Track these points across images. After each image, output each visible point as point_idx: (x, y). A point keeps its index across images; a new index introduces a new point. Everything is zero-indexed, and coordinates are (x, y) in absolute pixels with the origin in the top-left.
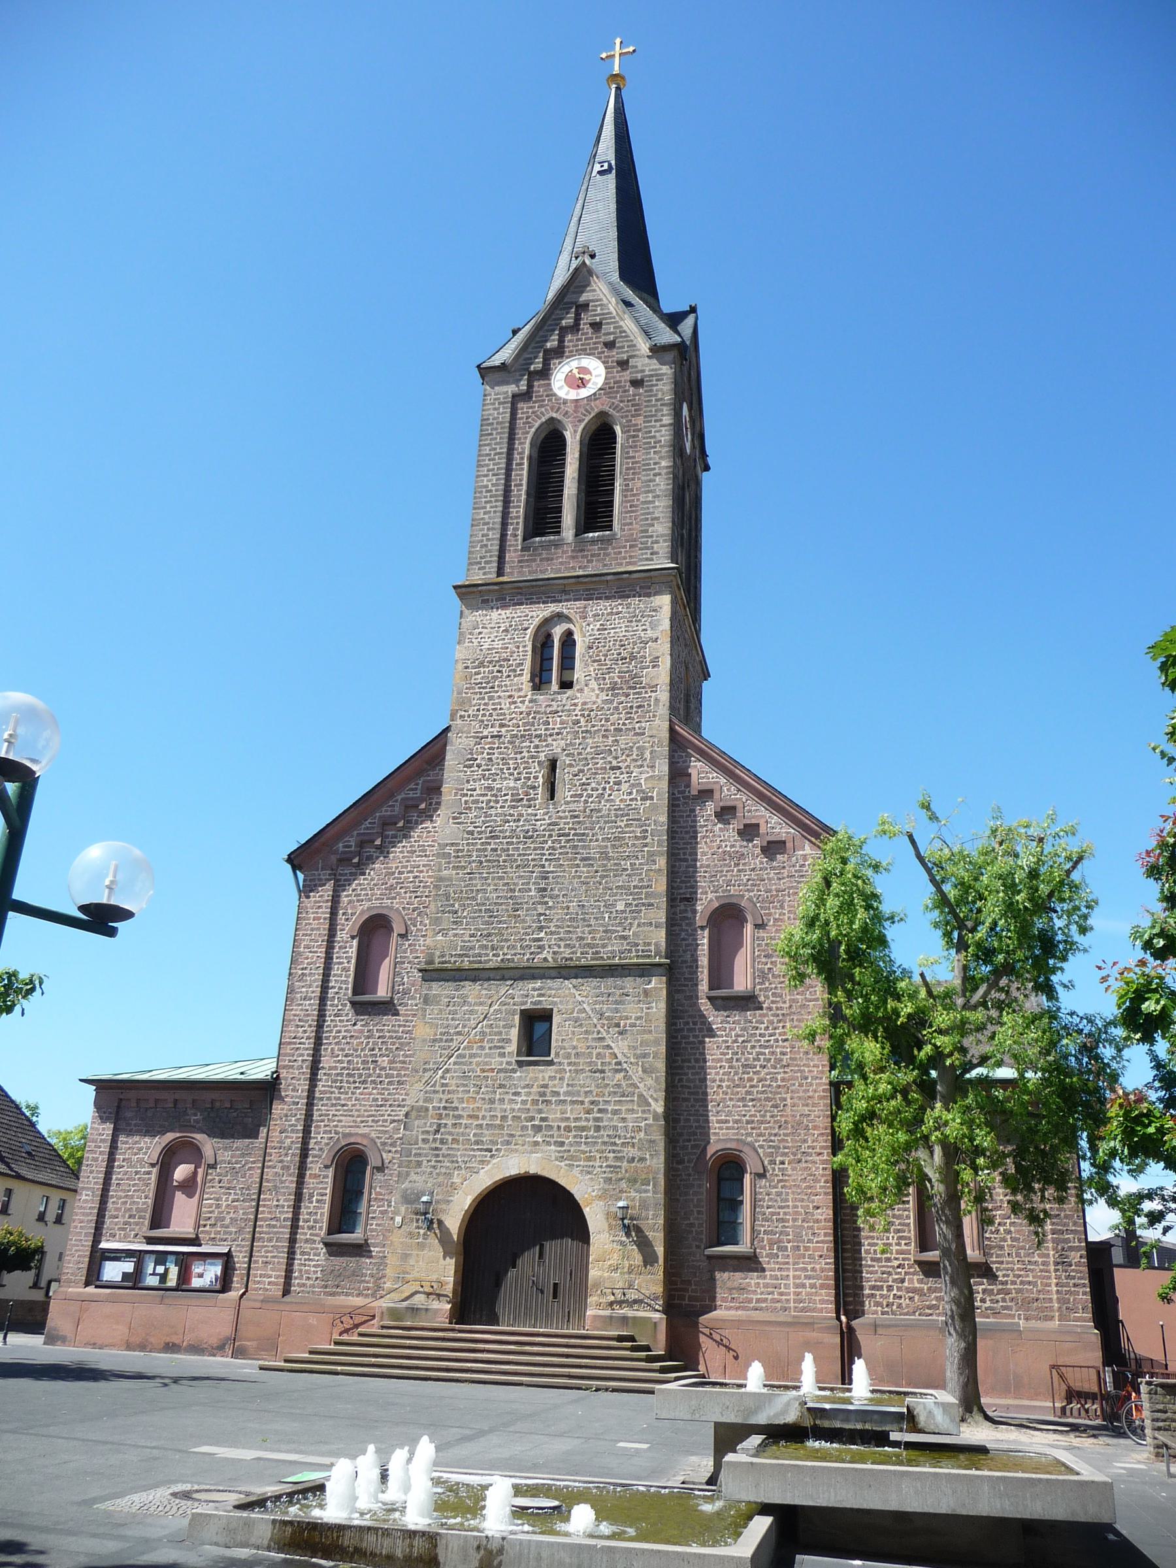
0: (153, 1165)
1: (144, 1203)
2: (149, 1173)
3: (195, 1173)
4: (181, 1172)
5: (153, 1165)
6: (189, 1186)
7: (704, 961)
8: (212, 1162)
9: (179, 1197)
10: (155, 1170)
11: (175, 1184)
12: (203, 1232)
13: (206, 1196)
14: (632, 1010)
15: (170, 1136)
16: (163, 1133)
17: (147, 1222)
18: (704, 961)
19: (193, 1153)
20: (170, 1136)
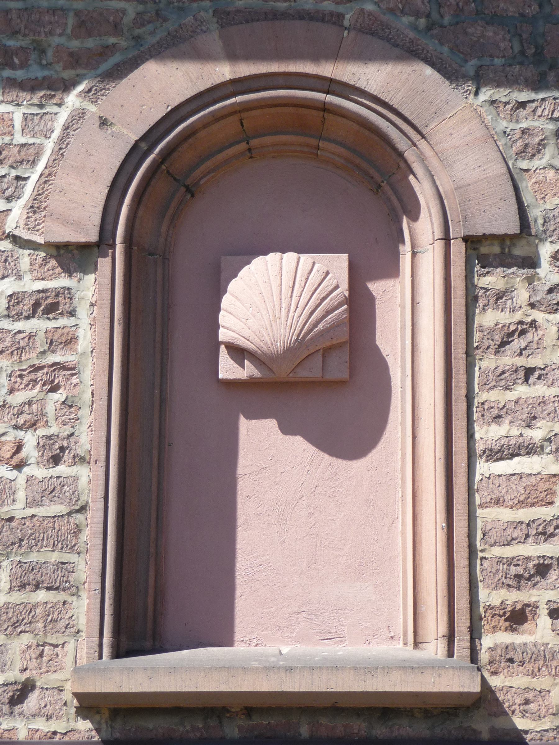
0: (74, 256)
1: (51, 491)
2: (49, 305)
3: (359, 307)
4: (267, 299)
5: (74, 256)
6: (329, 387)
7: (358, 99)
8: (506, 223)
9: (270, 458)
10: (94, 293)
11: (228, 369)
12: (508, 658)
13: (488, 434)
14: (238, 326)
15: (163, 85)
16: (109, 58)
17: (87, 609)
18: (358, 99)
19: (358, 185)
20: (163, 85)
